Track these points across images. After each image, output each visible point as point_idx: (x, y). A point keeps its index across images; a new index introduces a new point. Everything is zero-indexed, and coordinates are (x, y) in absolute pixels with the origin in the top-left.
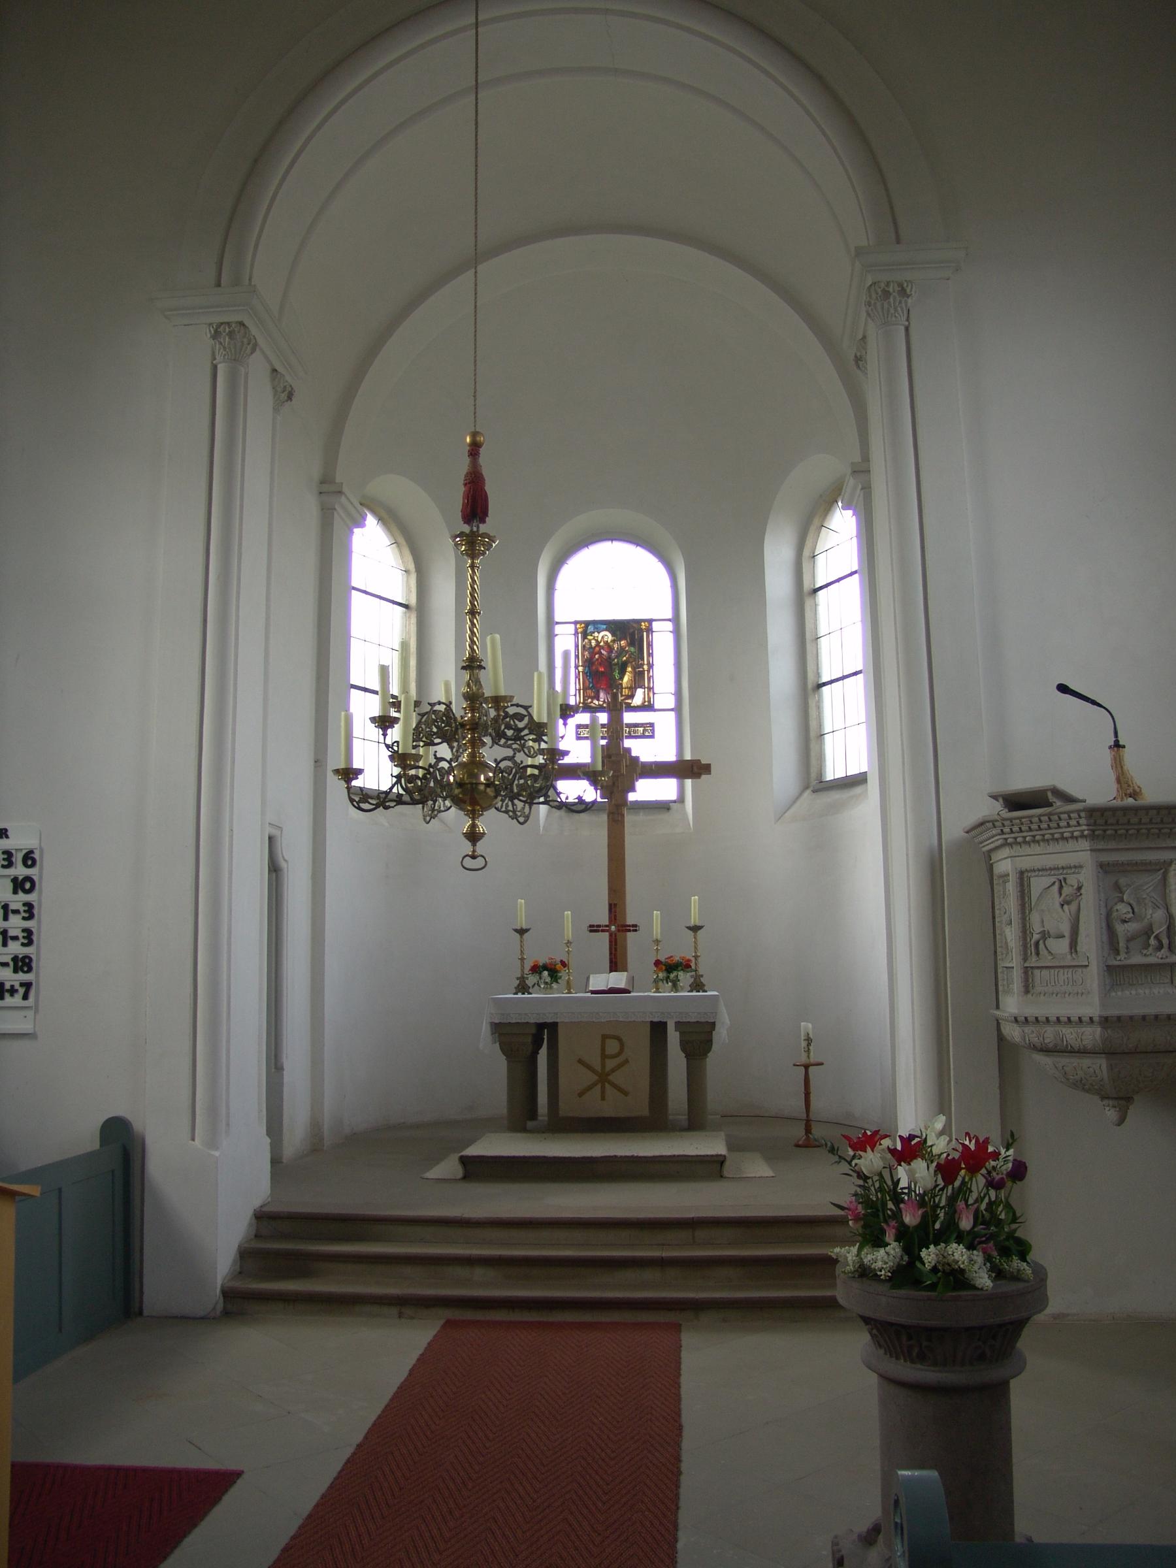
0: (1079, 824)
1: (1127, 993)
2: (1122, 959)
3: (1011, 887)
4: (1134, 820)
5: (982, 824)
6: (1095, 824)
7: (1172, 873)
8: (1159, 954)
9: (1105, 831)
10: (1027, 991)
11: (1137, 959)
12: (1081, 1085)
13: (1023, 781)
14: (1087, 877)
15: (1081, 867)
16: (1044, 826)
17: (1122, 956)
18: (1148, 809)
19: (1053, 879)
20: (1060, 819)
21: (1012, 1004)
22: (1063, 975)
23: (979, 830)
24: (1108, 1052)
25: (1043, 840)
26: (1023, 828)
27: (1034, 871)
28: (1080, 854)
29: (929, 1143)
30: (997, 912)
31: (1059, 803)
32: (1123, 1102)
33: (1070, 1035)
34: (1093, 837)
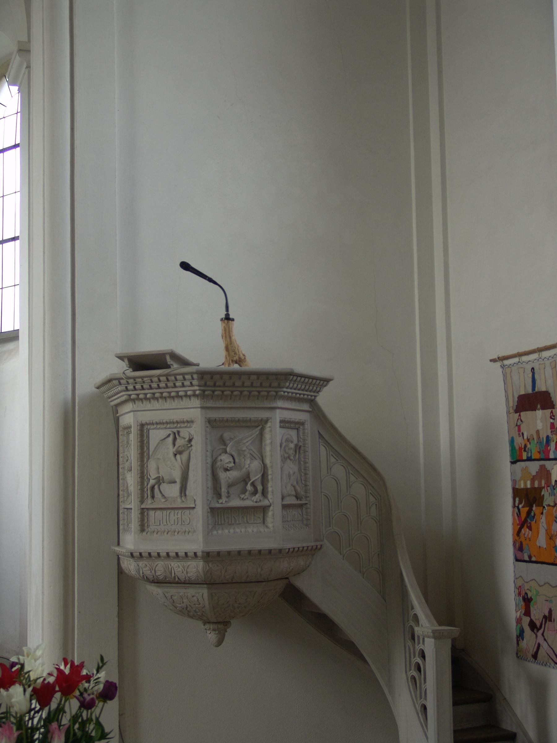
0: (192, 385)
1: (226, 531)
2: (224, 502)
3: (133, 437)
4: (238, 383)
5: (110, 381)
6: (205, 385)
7: (267, 430)
8: (255, 498)
9: (213, 391)
10: (142, 530)
11: (235, 503)
12: (188, 612)
13: (148, 346)
14: (197, 431)
15: (192, 422)
16: (162, 385)
17: (224, 499)
18: (249, 374)
19: (168, 432)
20: (176, 380)
21: (130, 541)
22: (174, 516)
23: (107, 386)
24: (209, 582)
25: (162, 397)
26: (145, 386)
27: (153, 424)
28: (191, 411)
29: (27, 669)
30: (121, 459)
31: (175, 366)
32: (221, 626)
33: (177, 568)
34: (203, 396)
